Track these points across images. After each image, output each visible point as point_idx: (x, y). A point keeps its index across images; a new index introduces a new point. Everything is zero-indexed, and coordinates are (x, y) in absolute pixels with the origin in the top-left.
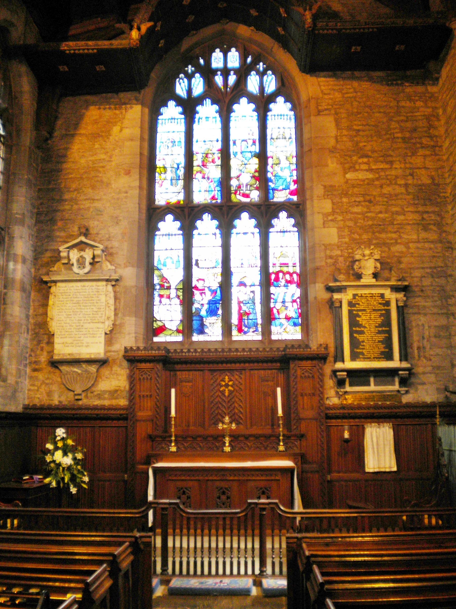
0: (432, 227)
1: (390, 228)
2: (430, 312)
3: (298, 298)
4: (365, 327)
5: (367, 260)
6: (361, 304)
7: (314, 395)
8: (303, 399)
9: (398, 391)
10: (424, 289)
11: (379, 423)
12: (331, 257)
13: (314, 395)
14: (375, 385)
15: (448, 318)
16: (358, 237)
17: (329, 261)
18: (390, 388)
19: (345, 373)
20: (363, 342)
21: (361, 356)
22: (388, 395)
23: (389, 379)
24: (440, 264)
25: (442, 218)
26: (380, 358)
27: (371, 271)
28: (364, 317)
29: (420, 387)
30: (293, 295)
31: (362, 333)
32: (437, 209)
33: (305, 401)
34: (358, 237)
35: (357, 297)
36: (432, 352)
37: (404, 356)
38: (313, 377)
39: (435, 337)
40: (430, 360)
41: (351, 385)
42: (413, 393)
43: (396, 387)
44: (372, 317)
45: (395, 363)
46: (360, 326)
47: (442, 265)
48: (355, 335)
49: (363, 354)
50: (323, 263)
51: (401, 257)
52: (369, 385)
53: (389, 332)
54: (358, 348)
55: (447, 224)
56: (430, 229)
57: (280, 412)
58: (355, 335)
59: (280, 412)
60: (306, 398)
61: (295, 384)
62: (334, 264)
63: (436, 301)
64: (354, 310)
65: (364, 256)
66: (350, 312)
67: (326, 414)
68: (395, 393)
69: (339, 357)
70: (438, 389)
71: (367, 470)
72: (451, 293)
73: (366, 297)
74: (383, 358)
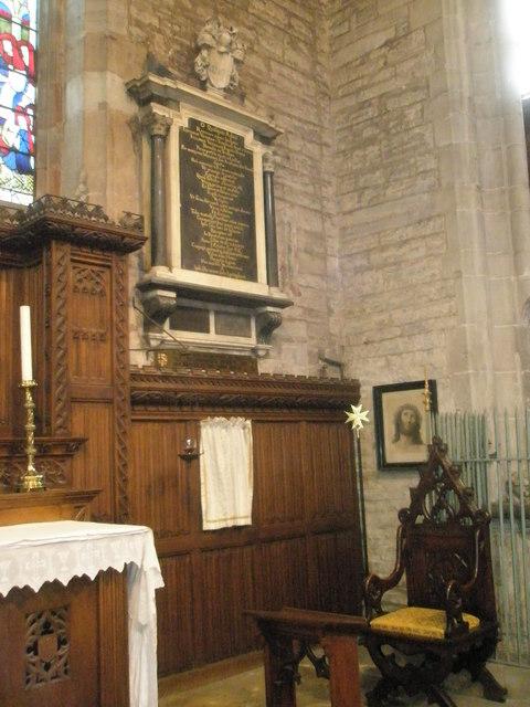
0: (301, 45)
1: (242, 16)
2: (299, 203)
3: (30, 106)
4: (211, 199)
5: (221, 53)
6: (205, 146)
7: (102, 338)
8: (78, 346)
9: (254, 350)
10: (291, 155)
11: (228, 416)
12: (139, 24)
13: (102, 338)
14: (217, 333)
15: (323, 221)
16: (190, 7)
17: (135, 30)
18: (241, 341)
19: (173, 295)
20: (207, 229)
21: (202, 261)
22: (236, 356)
23: (241, 321)
24: (312, 118)
25: (316, 38)
26: (236, 272)
27: (223, 82)
28: (209, 177)
29: (285, 346)
30: (18, 96)
31: (206, 209)
32: (309, 18)
33: (83, 355)
34: (190, 7)
35: (198, 129)
36: (302, 282)
37: (272, 280)
38: (102, 293)
39: (306, 251)
40: (300, 294)
41: (173, 327)
42: (275, 358)
43: (252, 341)
44: (224, 179)
45: (258, 288)
46: (202, 193)
47: (316, 122)
48: (194, 211)
49: (207, 258)
50: (124, 32)
51: (259, 81)
52: (207, 331)
53: (251, 220)
54: (197, 240)
55: (322, 51)
56: (301, 50)
57: (27, 375)
58: (194, 211)
59: (27, 375)
60: (83, 344)
61: (63, 306)
62: (146, 42)
63: (307, 185)
64: (192, 154)
65: (219, 43)
66: (184, 157)
67: (132, 397)
68: (247, 354)
69: (159, 255)
70: (310, 353)
71: (207, 526)
72: (326, 177)
73: (214, 133)
74: (241, 273)
